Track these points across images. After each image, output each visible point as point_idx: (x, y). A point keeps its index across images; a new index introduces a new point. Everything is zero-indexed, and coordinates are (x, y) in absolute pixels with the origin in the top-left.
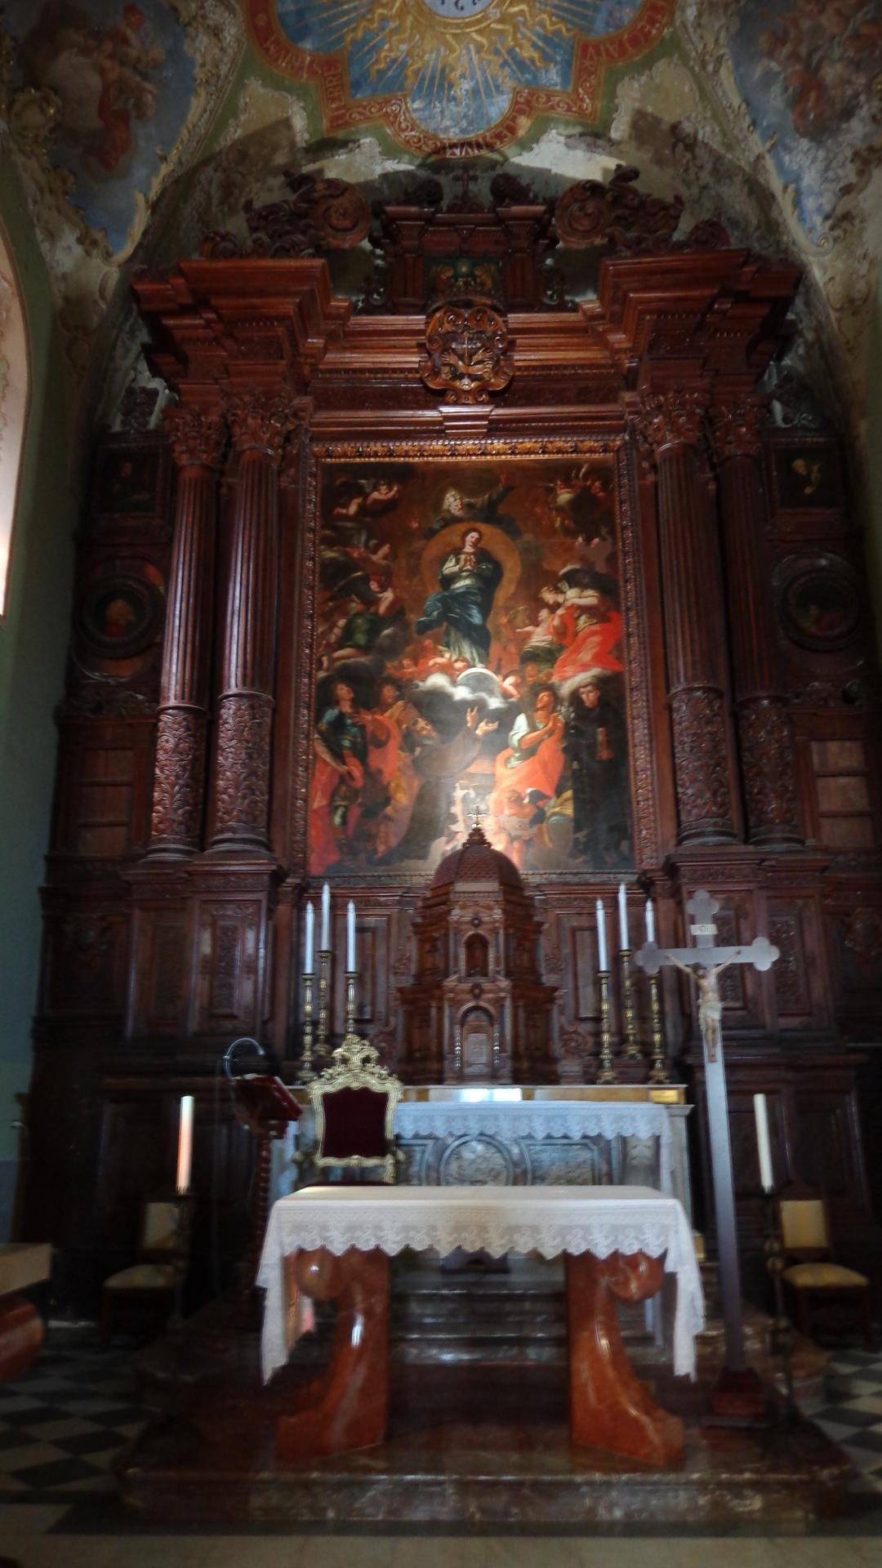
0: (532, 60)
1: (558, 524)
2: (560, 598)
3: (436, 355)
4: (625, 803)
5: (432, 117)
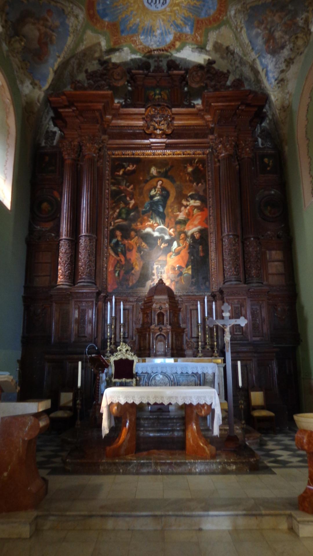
0: (181, 24)
1: (188, 178)
2: (188, 203)
3: (148, 122)
4: (208, 271)
5: (147, 41)
